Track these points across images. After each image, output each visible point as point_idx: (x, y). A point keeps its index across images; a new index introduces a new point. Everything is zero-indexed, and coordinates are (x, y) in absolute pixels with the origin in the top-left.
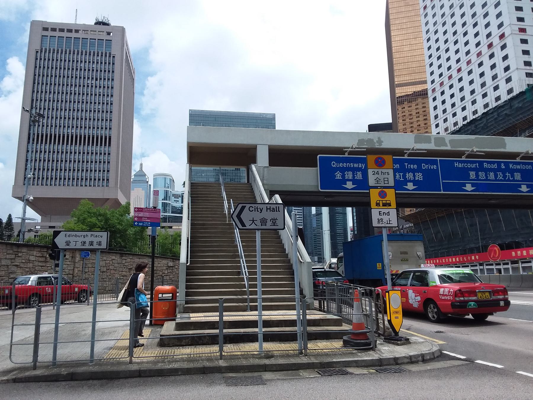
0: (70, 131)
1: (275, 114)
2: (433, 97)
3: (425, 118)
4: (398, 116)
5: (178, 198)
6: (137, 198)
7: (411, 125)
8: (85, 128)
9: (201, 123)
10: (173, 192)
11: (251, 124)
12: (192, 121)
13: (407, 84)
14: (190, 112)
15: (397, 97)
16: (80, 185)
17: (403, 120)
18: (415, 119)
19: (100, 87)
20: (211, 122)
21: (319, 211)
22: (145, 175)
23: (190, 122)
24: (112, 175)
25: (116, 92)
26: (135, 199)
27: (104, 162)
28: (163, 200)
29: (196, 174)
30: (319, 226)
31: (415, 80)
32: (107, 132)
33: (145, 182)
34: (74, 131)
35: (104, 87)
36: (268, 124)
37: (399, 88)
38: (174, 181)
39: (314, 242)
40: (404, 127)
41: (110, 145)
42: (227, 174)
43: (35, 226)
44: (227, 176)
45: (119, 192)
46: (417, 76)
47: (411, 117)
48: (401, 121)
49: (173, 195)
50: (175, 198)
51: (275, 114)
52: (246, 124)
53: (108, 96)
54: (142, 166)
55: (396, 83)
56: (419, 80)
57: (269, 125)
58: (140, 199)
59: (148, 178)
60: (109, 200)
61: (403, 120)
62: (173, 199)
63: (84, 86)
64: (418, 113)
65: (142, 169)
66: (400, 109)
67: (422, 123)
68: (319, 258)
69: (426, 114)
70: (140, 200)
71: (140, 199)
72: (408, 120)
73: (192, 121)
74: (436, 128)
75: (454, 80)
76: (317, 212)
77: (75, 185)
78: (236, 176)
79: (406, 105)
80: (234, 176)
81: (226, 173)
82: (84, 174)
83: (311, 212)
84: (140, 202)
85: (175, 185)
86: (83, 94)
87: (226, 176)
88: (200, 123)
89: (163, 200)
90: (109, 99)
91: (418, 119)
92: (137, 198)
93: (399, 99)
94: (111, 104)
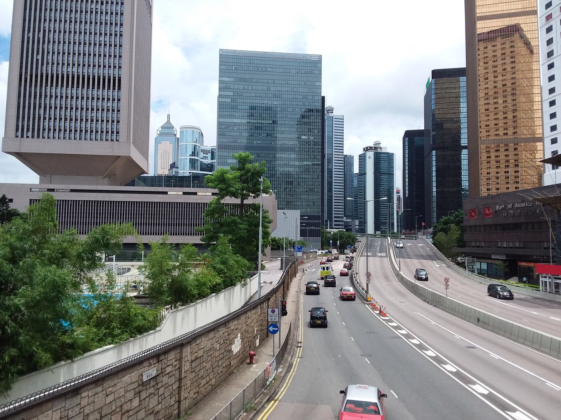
0: (70, 69)
1: (321, 55)
2: (547, 26)
3: (513, 60)
4: (478, 57)
5: (207, 154)
6: (164, 152)
7: (495, 69)
8: (94, 66)
9: (234, 66)
10: (202, 148)
11: (293, 67)
12: (223, 63)
13: (489, 17)
14: (221, 52)
15: (478, 34)
16: (104, 140)
17: (484, 63)
18: (500, 62)
19: (107, 13)
20: (245, 65)
21: (362, 170)
22: (173, 127)
23: (220, 65)
24: (122, 127)
25: (126, 19)
26: (162, 153)
27: (113, 110)
28: (190, 155)
29: (227, 127)
30: (362, 187)
31: (502, 12)
32: (116, 72)
33: (173, 135)
34: (75, 70)
35: (112, 13)
36: (312, 68)
37: (481, 22)
38: (202, 135)
39: (355, 203)
40: (486, 71)
41: (119, 88)
42: (263, 128)
43: (31, 189)
44: (263, 130)
45: (131, 148)
46: (505, 7)
47: (495, 59)
48: (482, 64)
49: (202, 151)
50: (204, 153)
51: (321, 55)
52: (287, 67)
53: (116, 24)
54: (169, 117)
55: (478, 15)
56: (508, 12)
57: (314, 68)
58: (168, 153)
59: (176, 130)
60: (120, 159)
61: (484, 63)
62: (202, 155)
63: (86, 12)
64: (504, 54)
65: (169, 121)
66: (481, 48)
67: (509, 67)
68: (360, 222)
69: (513, 56)
70: (168, 154)
71: (168, 153)
72: (491, 63)
73: (223, 63)
74: (549, 70)
75: (555, 20)
76: (361, 171)
77: (78, 138)
78: (273, 130)
79: (499, 41)
80: (271, 130)
81: (261, 127)
82: (89, 125)
83: (353, 172)
84: (168, 156)
85: (204, 139)
86: (86, 22)
87: (261, 130)
88: (232, 65)
89: (190, 155)
90: (118, 29)
91: (504, 61)
92: (164, 152)
93: (480, 36)
94: (121, 35)
